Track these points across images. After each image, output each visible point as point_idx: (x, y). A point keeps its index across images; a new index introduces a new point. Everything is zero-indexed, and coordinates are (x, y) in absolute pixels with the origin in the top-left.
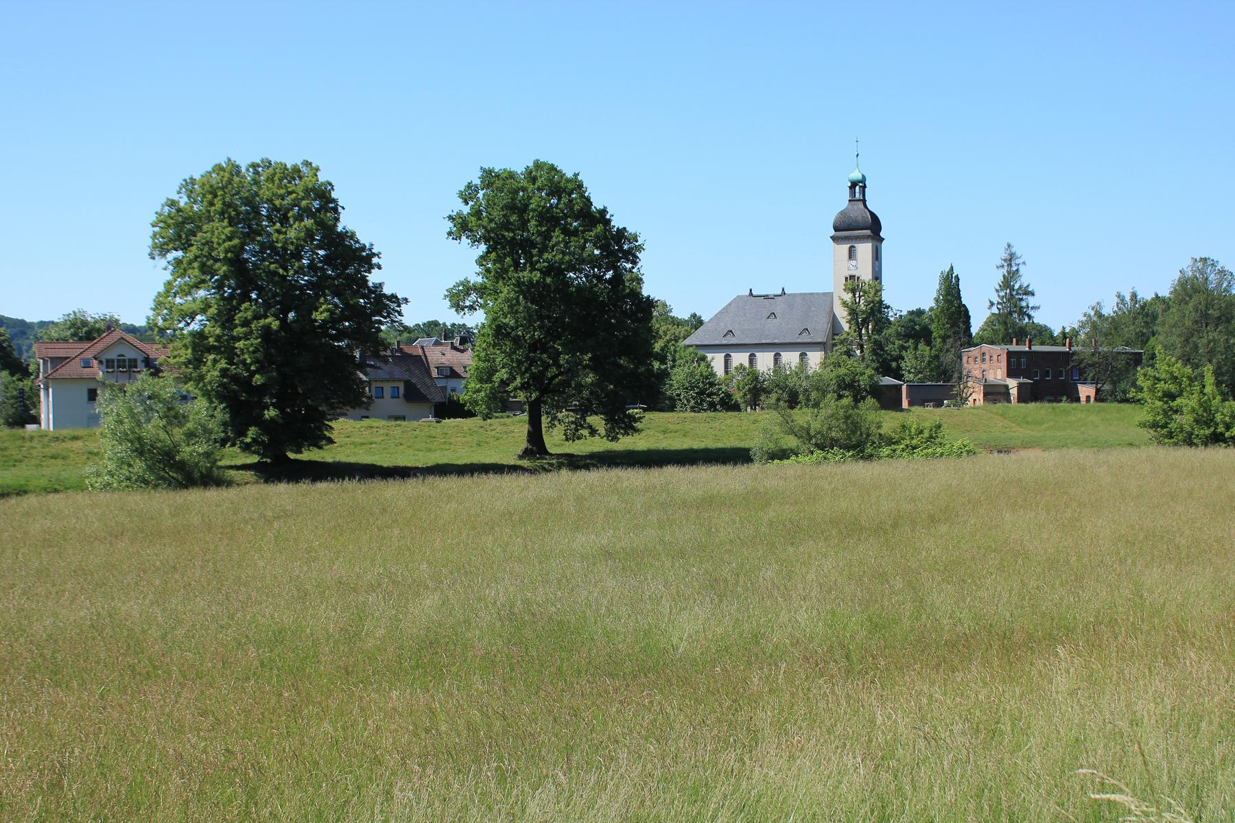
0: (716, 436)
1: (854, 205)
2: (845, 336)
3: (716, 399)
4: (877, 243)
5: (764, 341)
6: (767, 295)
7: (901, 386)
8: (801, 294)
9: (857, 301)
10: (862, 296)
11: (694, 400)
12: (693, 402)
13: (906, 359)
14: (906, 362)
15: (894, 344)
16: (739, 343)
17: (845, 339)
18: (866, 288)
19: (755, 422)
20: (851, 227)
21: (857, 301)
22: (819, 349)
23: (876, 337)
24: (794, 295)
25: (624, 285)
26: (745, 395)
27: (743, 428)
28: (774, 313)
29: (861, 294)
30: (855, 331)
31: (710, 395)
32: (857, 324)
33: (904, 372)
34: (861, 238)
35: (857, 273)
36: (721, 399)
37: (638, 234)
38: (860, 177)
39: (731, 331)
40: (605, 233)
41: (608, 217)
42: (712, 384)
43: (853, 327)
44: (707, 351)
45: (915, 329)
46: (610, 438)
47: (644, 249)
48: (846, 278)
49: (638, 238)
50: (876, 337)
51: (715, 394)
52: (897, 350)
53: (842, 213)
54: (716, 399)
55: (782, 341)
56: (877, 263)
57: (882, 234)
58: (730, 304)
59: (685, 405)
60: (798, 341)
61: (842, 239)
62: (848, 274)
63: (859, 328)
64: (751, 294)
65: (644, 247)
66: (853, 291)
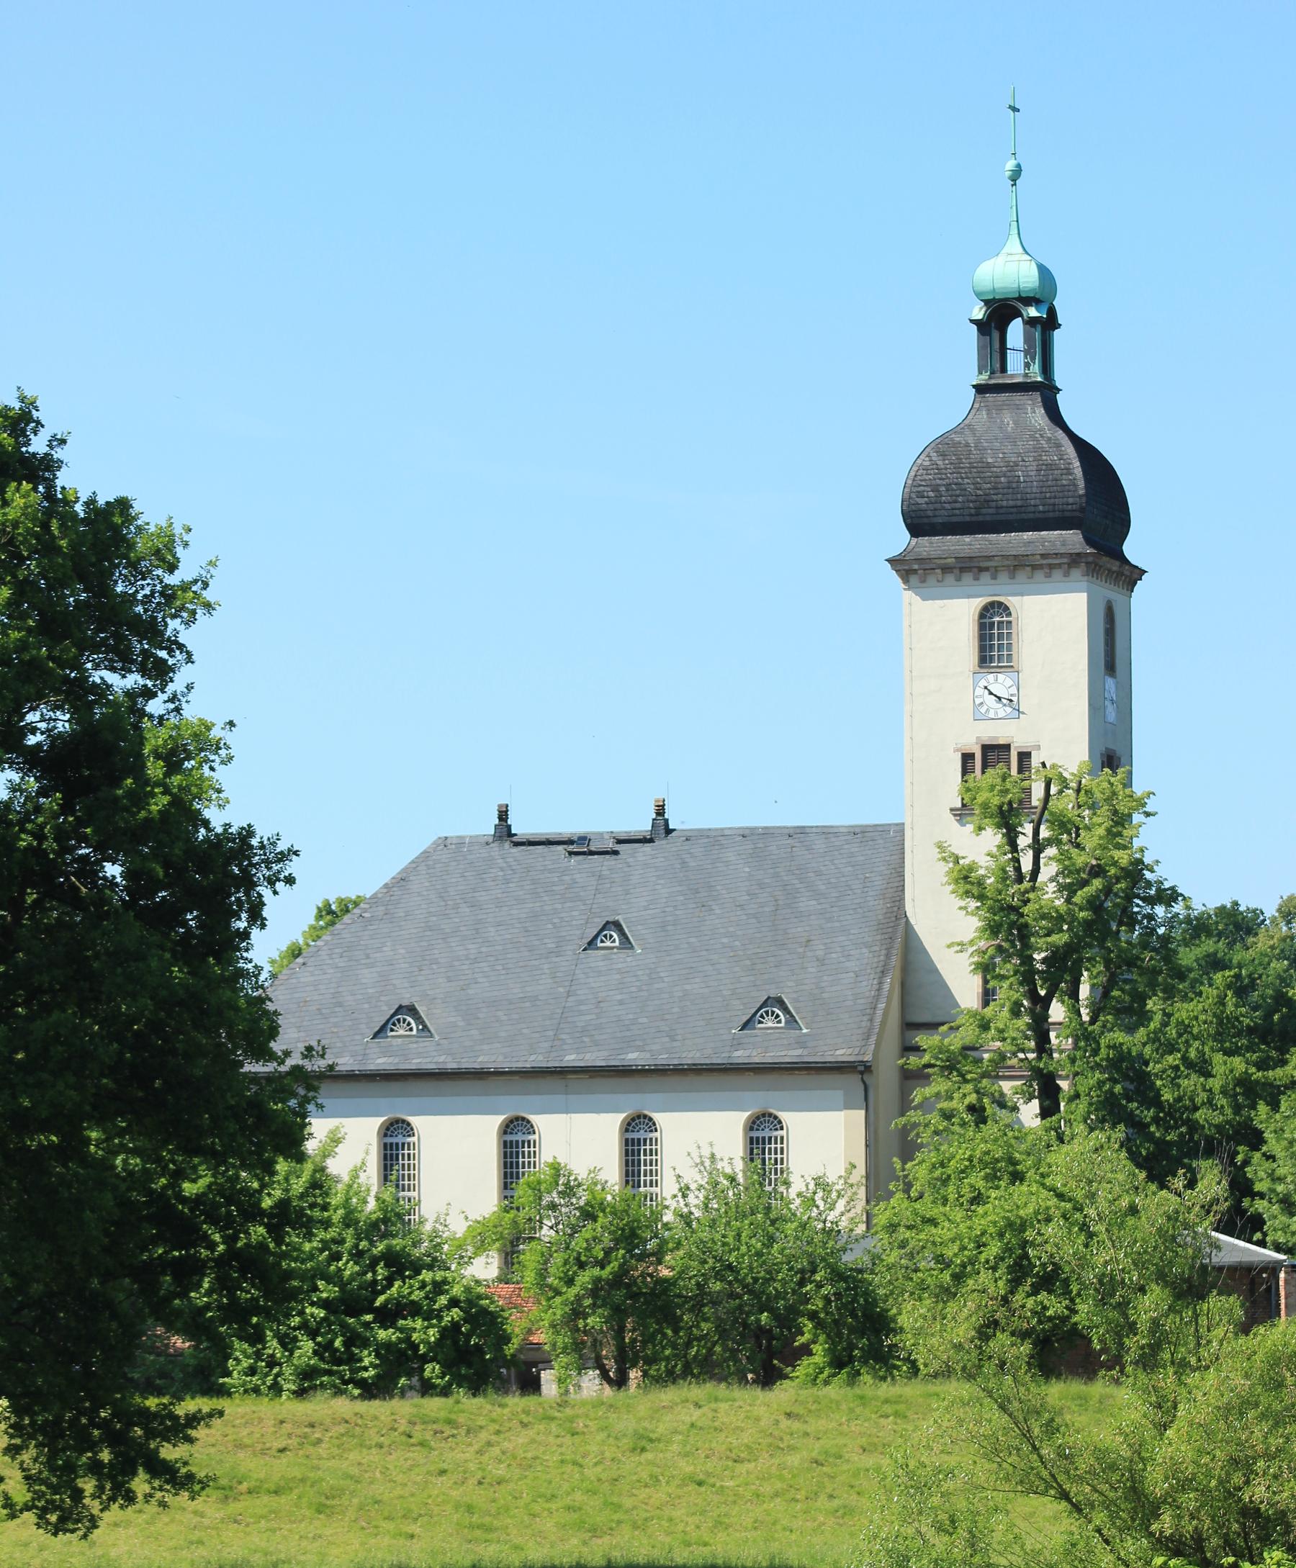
0: (470, 1509)
2: (967, 1034)
3: (424, 1333)
4: (1109, 592)
5: (571, 1059)
6: (583, 839)
7: (1273, 1268)
8: (746, 834)
9: (1026, 865)
10: (1049, 842)
11: (313, 1334)
12: (307, 1346)
14: (1270, 1157)
15: (1203, 1068)
16: (452, 1065)
18: (1065, 803)
19: (642, 1443)
20: (988, 514)
21: (1026, 865)
22: (839, 1095)
23: (1119, 1037)
24: (713, 839)
25: (142, 780)
26: (577, 1313)
27: (591, 1473)
29: (1045, 833)
30: (1016, 1012)
31: (387, 1316)
32: (1028, 977)
33: (1260, 1205)
34: (1035, 567)
35: (1016, 735)
36: (444, 1332)
37: (178, 530)
39: (412, 1011)
40: (46, 526)
41: (38, 445)
42: (400, 1265)
43: (1007, 992)
44: (658, 1097)
46: (53, 1518)
47: (208, 606)
48: (967, 758)
49: (179, 551)
50: (1119, 1037)
51: (414, 1310)
53: (944, 446)
54: (424, 1333)
55: (663, 1059)
56: (1110, 682)
57: (1133, 549)
58: (401, 881)
59: (272, 1363)
61: (946, 569)
62: (972, 737)
63: (1033, 995)
64: (504, 831)
65: (208, 595)
66: (1007, 819)
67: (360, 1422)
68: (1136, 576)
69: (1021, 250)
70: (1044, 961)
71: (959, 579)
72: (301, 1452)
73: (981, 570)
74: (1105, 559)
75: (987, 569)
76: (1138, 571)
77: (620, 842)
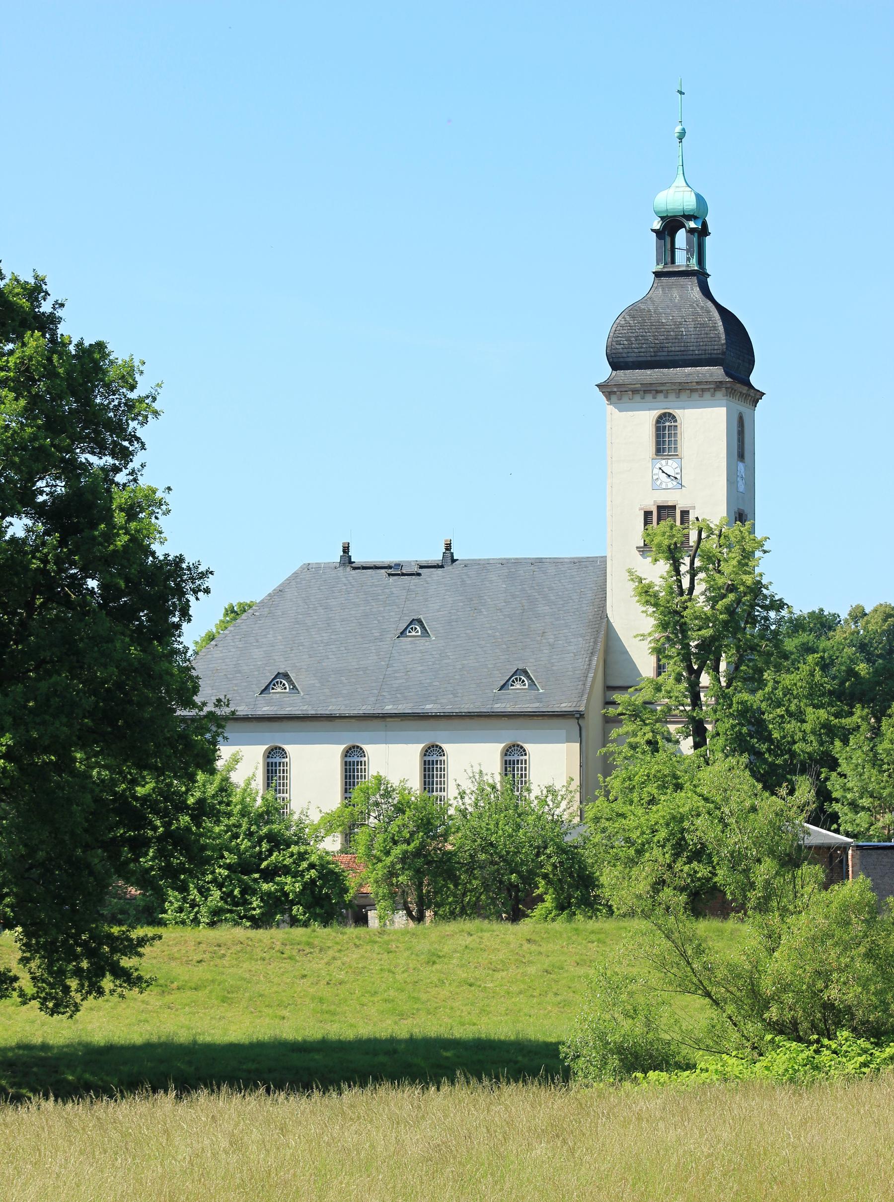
0: (321, 1000)
1: (670, 287)
2: (647, 694)
3: (292, 886)
4: (741, 407)
5: (389, 708)
6: (398, 565)
7: (844, 848)
9: (686, 584)
10: (701, 569)
12: (217, 894)
13: (844, 767)
17: (645, 703)
18: (711, 544)
19: (433, 958)
20: (662, 356)
21: (686, 584)
23: (745, 696)
24: (483, 566)
25: (111, 525)
26: (392, 873)
28: (420, 622)
29: (698, 563)
31: (269, 875)
32: (686, 657)
33: (836, 807)
34: (692, 390)
36: (305, 886)
37: (136, 363)
38: (688, 202)
39: (286, 676)
40: (50, 360)
41: (46, 307)
42: (277, 842)
43: (674, 666)
44: (288, 735)
45: (856, 675)
48: (648, 514)
49: (137, 377)
50: (745, 696)
51: (286, 871)
52: (812, 738)
53: (634, 311)
54: (292, 886)
55: (448, 709)
56: (741, 466)
57: (755, 379)
58: (280, 591)
60: (499, 707)
61: (635, 391)
62: (651, 504)
63: (690, 669)
65: (156, 406)
66: (673, 554)
67: (250, 943)
68: (758, 397)
69: (685, 184)
70: (696, 647)
71: (643, 398)
72: (212, 963)
73: (657, 392)
74: (739, 385)
75: (661, 391)
76: (758, 393)
77: (421, 567)
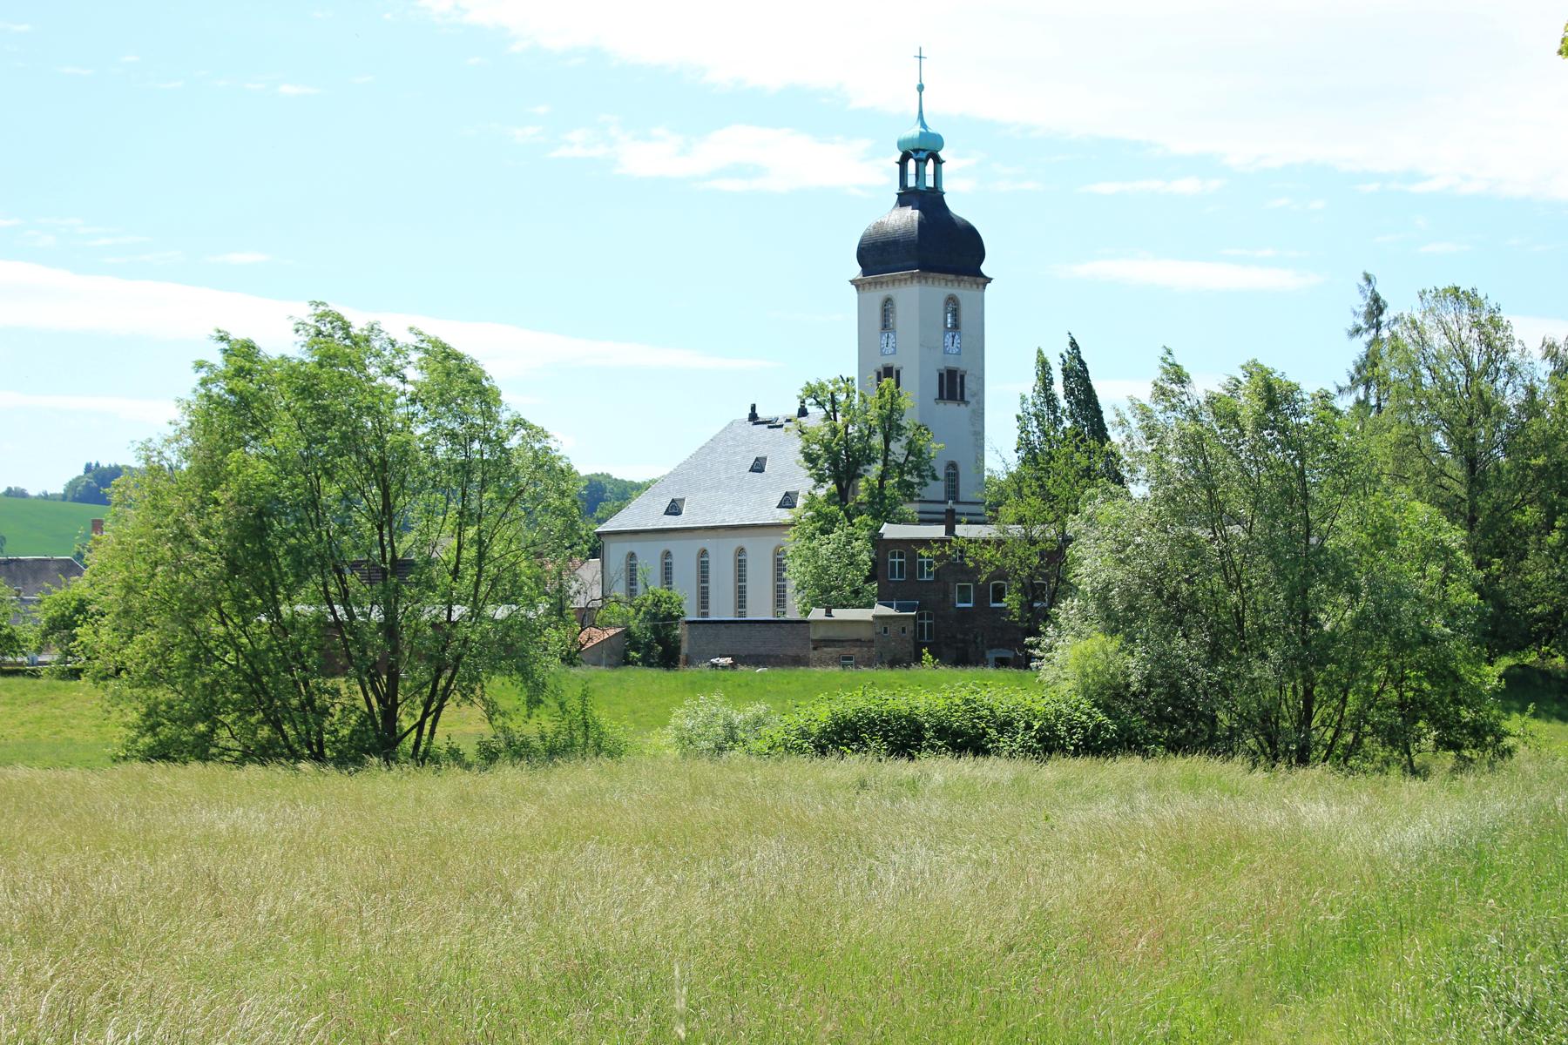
57: (985, 268)
73: (882, 283)
